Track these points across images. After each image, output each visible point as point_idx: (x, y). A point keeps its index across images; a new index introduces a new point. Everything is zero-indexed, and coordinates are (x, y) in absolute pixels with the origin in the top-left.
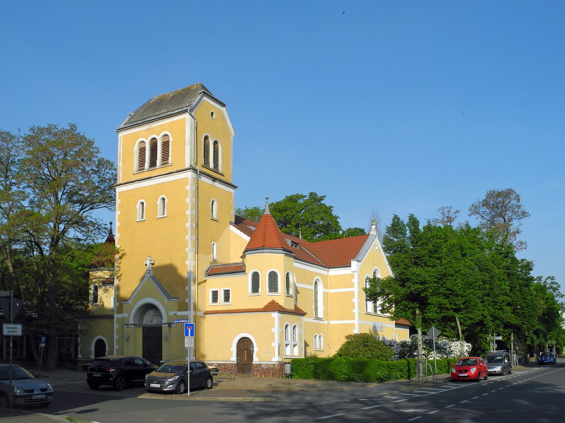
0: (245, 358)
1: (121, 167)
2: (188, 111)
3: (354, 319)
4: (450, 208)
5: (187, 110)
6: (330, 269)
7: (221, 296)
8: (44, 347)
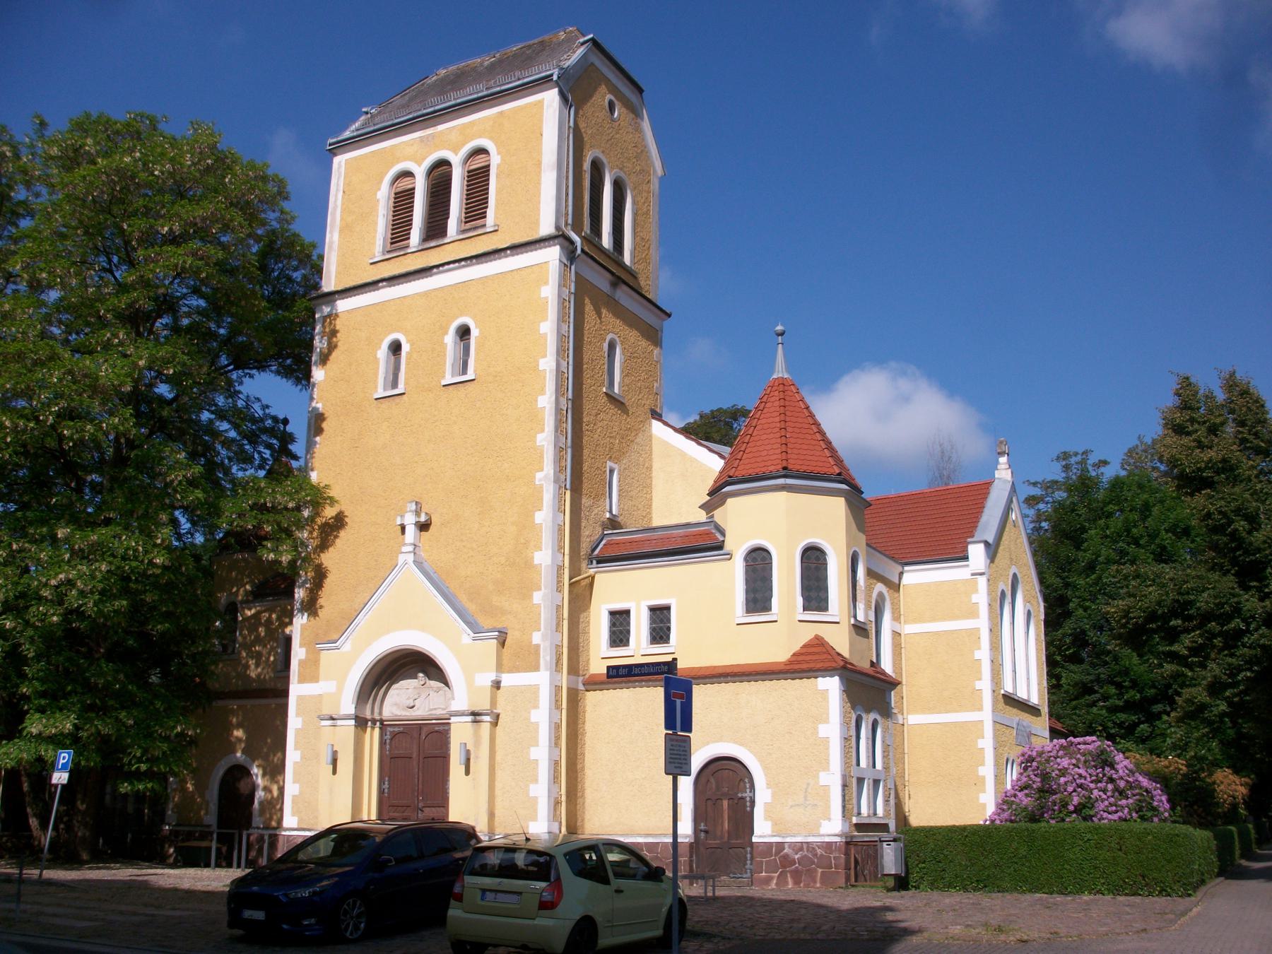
0: (722, 823)
1: (336, 246)
2: (555, 78)
3: (980, 709)
4: (1085, 453)
5: (552, 75)
6: (906, 568)
7: (640, 626)
8: (63, 786)
